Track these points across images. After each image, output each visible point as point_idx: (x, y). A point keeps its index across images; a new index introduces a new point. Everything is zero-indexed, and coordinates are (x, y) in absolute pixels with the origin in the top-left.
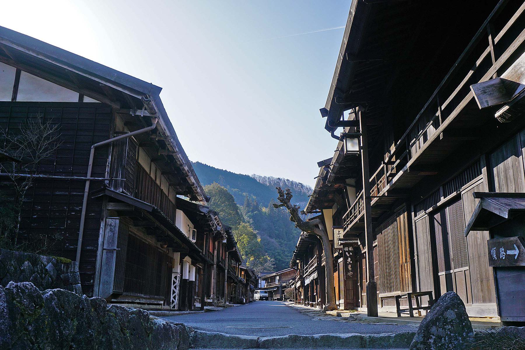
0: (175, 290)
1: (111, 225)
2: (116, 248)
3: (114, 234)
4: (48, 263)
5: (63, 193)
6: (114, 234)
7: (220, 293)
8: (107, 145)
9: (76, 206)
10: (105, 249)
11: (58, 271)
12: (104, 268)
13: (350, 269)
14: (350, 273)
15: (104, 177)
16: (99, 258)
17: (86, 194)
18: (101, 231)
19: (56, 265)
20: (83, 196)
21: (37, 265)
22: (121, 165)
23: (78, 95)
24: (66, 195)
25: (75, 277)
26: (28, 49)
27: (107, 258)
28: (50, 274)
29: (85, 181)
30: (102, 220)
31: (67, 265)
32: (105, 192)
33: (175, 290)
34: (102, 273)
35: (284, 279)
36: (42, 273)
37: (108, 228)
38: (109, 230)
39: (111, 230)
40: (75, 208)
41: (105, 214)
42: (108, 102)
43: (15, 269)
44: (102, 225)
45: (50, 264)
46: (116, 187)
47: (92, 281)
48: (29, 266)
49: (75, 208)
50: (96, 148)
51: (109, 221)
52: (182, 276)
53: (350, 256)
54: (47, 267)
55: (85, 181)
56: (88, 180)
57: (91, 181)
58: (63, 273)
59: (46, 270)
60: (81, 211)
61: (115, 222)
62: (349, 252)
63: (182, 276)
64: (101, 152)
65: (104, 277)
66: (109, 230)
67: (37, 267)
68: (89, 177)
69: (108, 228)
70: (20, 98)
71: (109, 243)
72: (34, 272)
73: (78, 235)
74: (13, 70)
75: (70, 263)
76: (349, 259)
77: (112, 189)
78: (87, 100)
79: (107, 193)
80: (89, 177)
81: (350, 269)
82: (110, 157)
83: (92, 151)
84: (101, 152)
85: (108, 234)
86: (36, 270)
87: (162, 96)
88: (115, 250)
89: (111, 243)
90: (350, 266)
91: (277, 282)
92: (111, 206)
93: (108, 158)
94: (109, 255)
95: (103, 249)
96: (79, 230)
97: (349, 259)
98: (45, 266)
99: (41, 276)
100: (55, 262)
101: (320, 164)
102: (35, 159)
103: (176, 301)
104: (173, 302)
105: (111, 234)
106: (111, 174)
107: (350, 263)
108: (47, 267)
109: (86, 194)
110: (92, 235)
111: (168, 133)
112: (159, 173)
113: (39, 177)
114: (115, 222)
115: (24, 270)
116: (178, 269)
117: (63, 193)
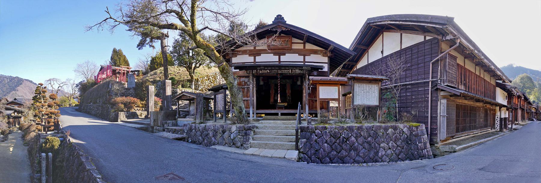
0: (498, 123)
7: (523, 118)
8: (438, 60)
12: (441, 125)
16: (439, 120)
19: (410, 128)
23: (423, 37)
26: (396, 21)
29: (429, 82)
31: (417, 127)
33: (498, 123)
38: (442, 105)
42: (436, 36)
43: (383, 133)
50: (433, 64)
55: (429, 82)
57: (432, 82)
58: (415, 131)
61: (444, 101)
64: (435, 64)
66: (442, 105)
68: (430, 79)
70: (403, 48)
74: (398, 35)
75: (419, 126)
78: (428, 38)
79: (438, 87)
83: (431, 65)
84: (435, 64)
87: (455, 20)
89: (444, 112)
92: (442, 93)
103: (498, 127)
110: (434, 109)
111: (472, 48)
112: (482, 71)
116: (498, 114)
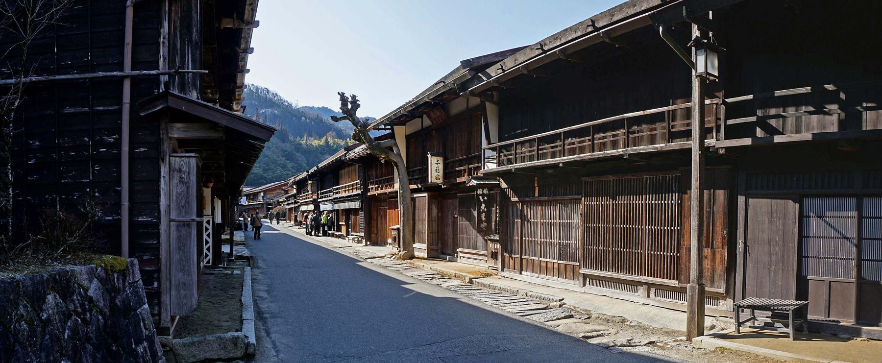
1: (180, 171)
2: (195, 217)
3: (188, 188)
4: (91, 281)
5: (78, 109)
6: (188, 188)
9: (108, 135)
10: (173, 220)
11: (110, 294)
12: (176, 257)
13: (484, 219)
14: (484, 225)
15: (157, 68)
17: (126, 109)
18: (162, 185)
19: (105, 281)
20: (120, 112)
21: (73, 294)
22: (190, 40)
24: (86, 112)
25: (137, 292)
27: (179, 238)
28: (98, 307)
29: (120, 80)
30: (163, 160)
32: (167, 101)
34: (173, 267)
35: (268, 196)
36: (84, 311)
37: (176, 176)
39: (181, 180)
40: (106, 138)
41: (166, 147)
43: (30, 324)
44: (164, 170)
45: (95, 281)
46: (183, 88)
47: (156, 285)
48: (57, 305)
49: (106, 138)
51: (177, 161)
52: (213, 219)
53: (485, 202)
54: (91, 293)
55: (120, 80)
56: (127, 77)
57: (133, 79)
59: (90, 300)
60: (118, 144)
62: (483, 195)
63: (213, 219)
65: (177, 276)
67: (73, 301)
68: (128, 71)
69: (176, 176)
71: (180, 208)
72: (69, 316)
73: (119, 194)
76: (483, 205)
77: (176, 92)
79: (172, 103)
80: (128, 71)
81: (484, 219)
82: (166, 24)
85: (177, 189)
86: (72, 307)
88: (193, 220)
90: (484, 215)
91: (260, 198)
92: (177, 131)
93: (161, 25)
94: (183, 231)
95: (171, 220)
96: (119, 183)
97: (483, 205)
98: (86, 290)
99: (84, 320)
100: (103, 274)
101: (249, 70)
102: (25, 31)
104: (207, 255)
105: (181, 188)
106: (171, 62)
107: (484, 211)
108: (91, 293)
109: (126, 109)
113: (31, 82)
114: (189, 163)
115: (49, 319)
117: (78, 109)
